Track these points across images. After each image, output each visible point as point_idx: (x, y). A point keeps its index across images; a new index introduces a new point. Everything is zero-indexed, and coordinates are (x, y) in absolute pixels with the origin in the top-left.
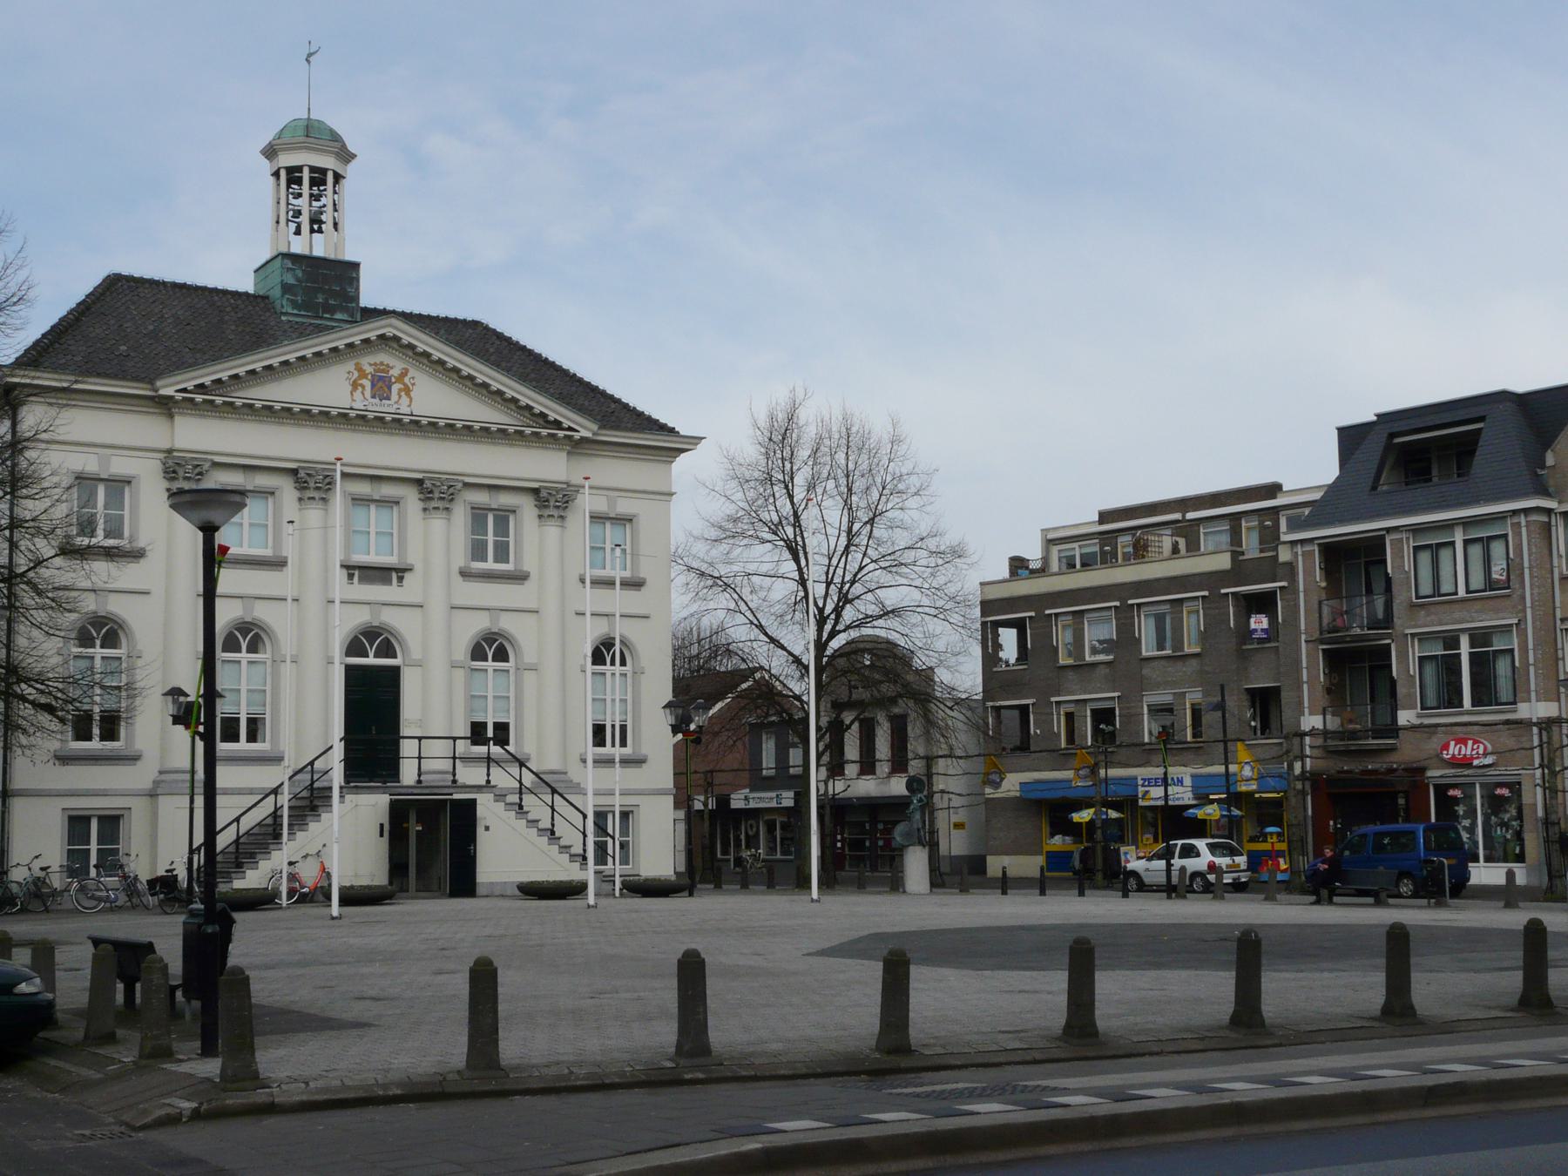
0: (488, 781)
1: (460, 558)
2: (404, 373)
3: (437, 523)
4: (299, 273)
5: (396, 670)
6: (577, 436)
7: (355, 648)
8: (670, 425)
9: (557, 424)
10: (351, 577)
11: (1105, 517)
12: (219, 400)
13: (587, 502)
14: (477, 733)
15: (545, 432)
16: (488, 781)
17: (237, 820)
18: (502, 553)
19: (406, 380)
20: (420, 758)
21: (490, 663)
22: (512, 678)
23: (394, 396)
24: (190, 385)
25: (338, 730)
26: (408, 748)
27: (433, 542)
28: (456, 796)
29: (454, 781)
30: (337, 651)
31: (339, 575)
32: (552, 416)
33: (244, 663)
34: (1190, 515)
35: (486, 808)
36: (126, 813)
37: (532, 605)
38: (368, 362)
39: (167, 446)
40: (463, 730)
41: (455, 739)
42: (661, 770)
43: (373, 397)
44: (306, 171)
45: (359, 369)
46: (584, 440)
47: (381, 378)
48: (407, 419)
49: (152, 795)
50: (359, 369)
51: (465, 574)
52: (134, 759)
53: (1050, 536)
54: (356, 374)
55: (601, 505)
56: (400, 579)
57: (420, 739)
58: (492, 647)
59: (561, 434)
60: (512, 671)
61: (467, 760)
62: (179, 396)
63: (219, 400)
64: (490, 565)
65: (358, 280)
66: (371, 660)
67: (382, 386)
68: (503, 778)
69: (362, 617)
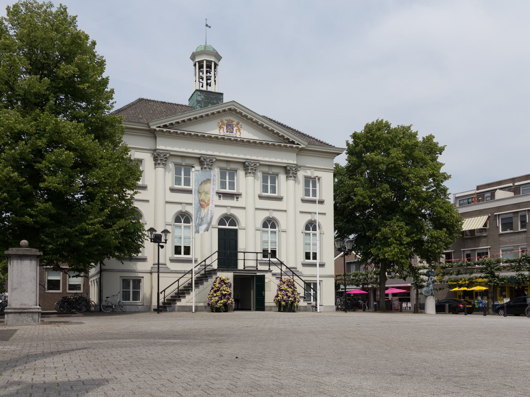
0: (269, 269)
1: (259, 190)
2: (238, 124)
3: (250, 178)
4: (203, 97)
5: (236, 231)
6: (300, 147)
7: (221, 222)
8: (333, 145)
9: (293, 142)
10: (220, 197)
11: (478, 188)
12: (172, 131)
13: (301, 174)
14: (265, 253)
15: (288, 145)
16: (269, 269)
17: (178, 280)
18: (273, 190)
19: (239, 126)
20: (244, 260)
21: (269, 229)
22: (277, 234)
23: (235, 132)
24: (161, 125)
25: (216, 248)
26: (240, 256)
27: (248, 185)
28: (258, 274)
29: (257, 269)
30: (215, 222)
31: (216, 197)
32: (291, 140)
33: (183, 227)
34: (516, 184)
35: (268, 276)
36: (142, 279)
37: (284, 209)
38: (225, 119)
39: (154, 148)
40: (260, 250)
41: (257, 253)
42: (330, 269)
43: (227, 132)
44: (205, 62)
45: (222, 122)
46: (302, 149)
47: (230, 125)
48: (239, 139)
49: (151, 273)
50: (222, 122)
51: (261, 197)
52: (144, 260)
53: (457, 196)
54: (221, 124)
55: (309, 173)
56: (237, 198)
57: (244, 253)
58: (270, 223)
59: (294, 146)
60: (277, 232)
61: (261, 264)
62: (158, 129)
63: (172, 131)
64: (269, 194)
65: (223, 99)
66: (227, 227)
67: (230, 126)
68: (276, 270)
69: (224, 211)
